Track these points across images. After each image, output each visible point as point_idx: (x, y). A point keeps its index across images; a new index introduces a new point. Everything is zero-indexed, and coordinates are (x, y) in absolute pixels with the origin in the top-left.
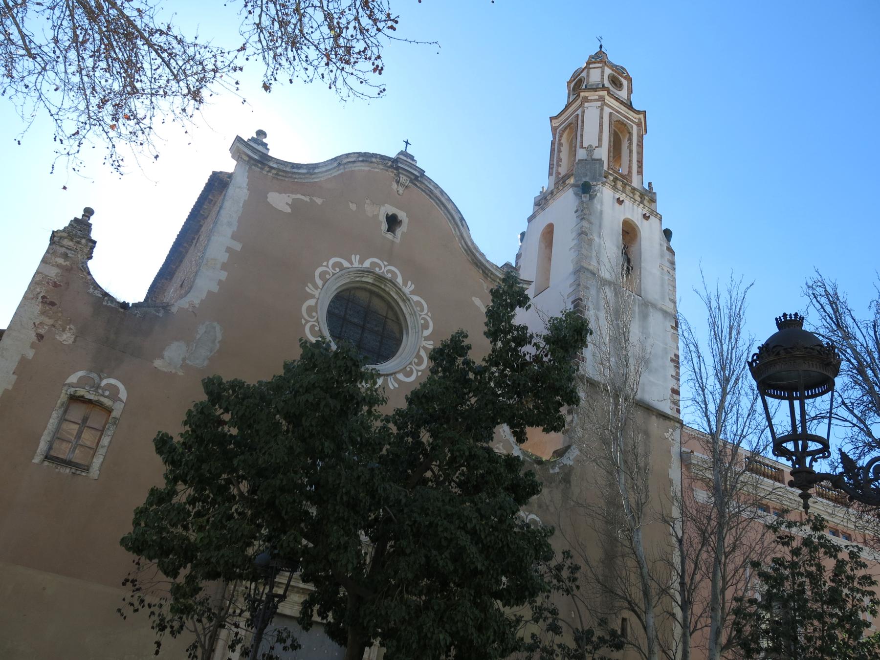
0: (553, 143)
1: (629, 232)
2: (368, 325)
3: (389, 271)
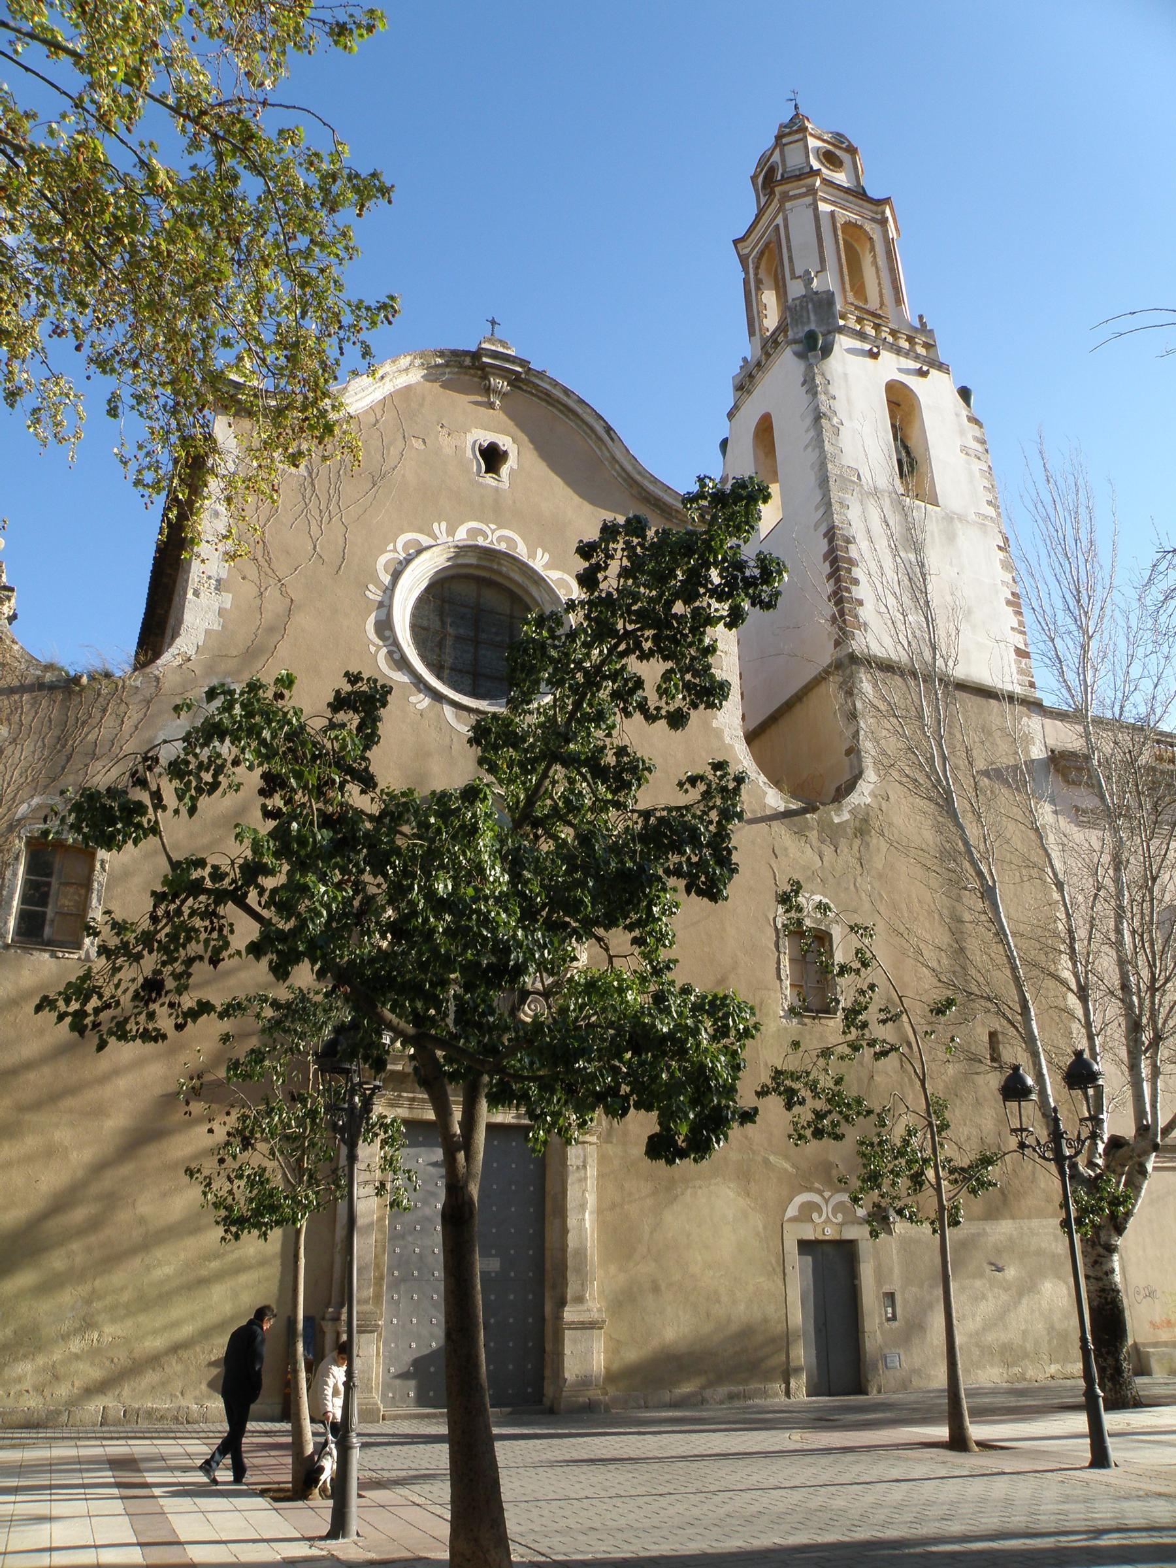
0: (746, 282)
1: (900, 404)
2: (484, 636)
3: (500, 539)
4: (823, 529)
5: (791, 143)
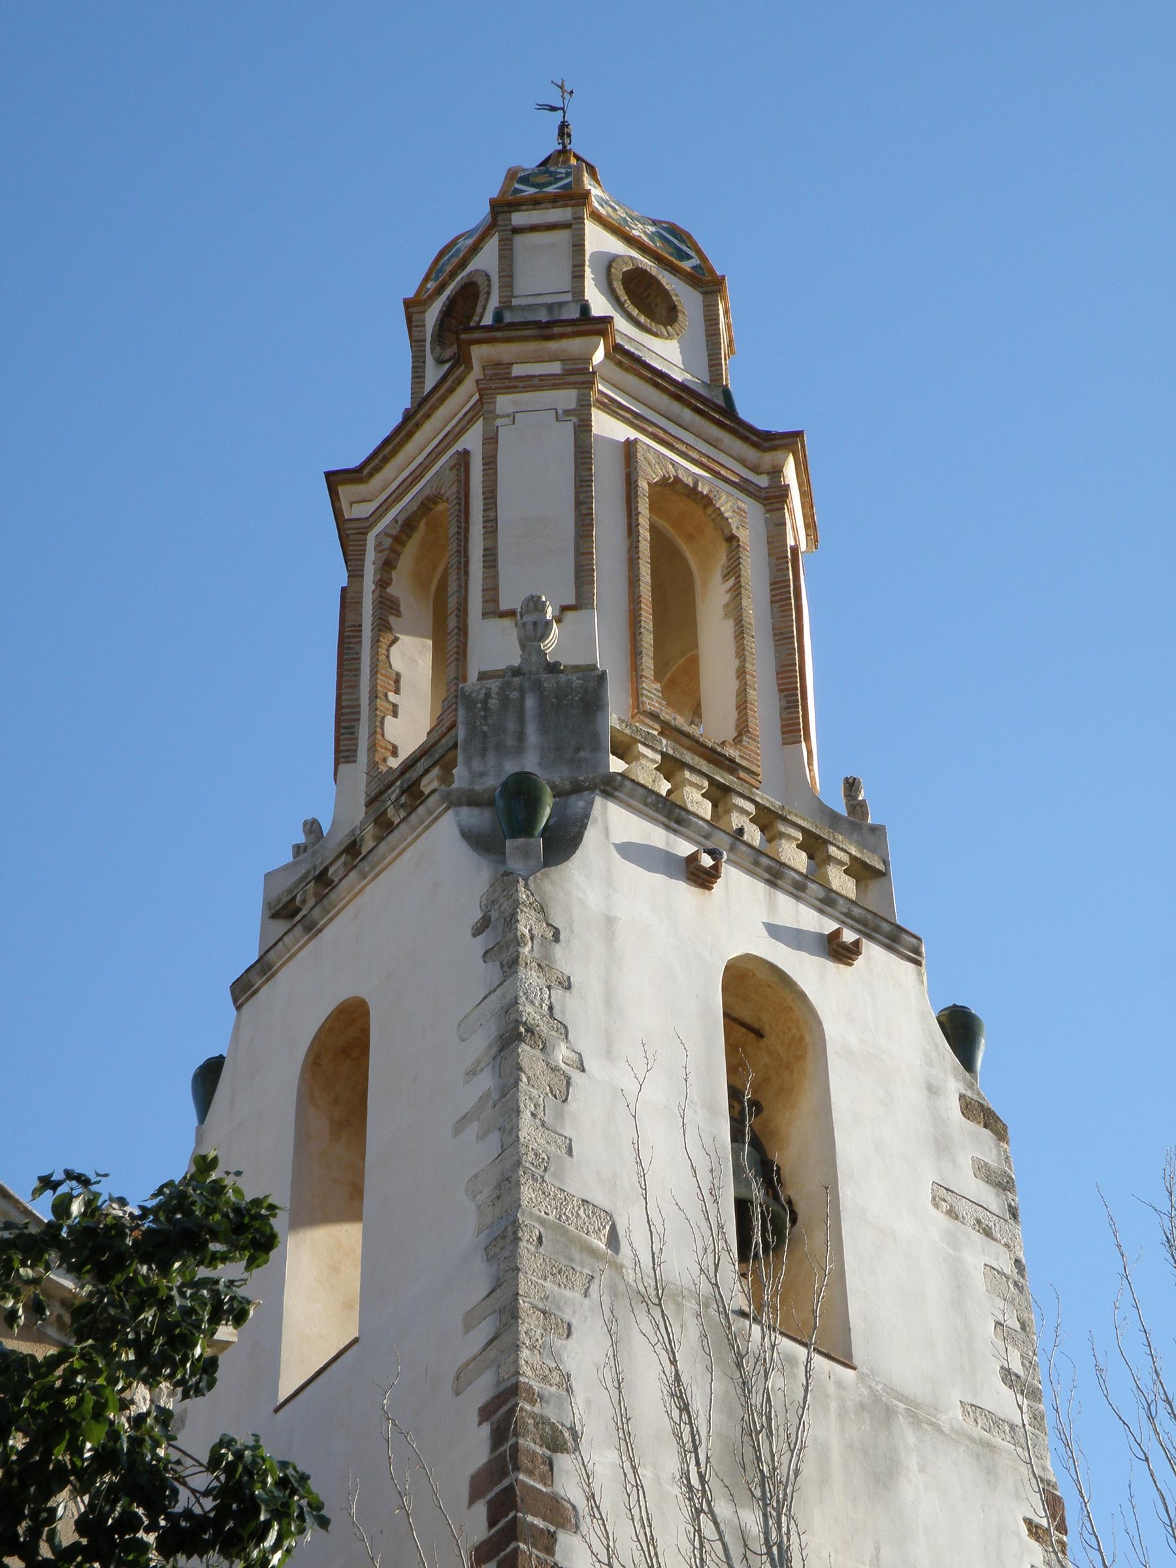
0: (349, 601)
1: (763, 1031)
4: (482, 1390)
5: (534, 228)
